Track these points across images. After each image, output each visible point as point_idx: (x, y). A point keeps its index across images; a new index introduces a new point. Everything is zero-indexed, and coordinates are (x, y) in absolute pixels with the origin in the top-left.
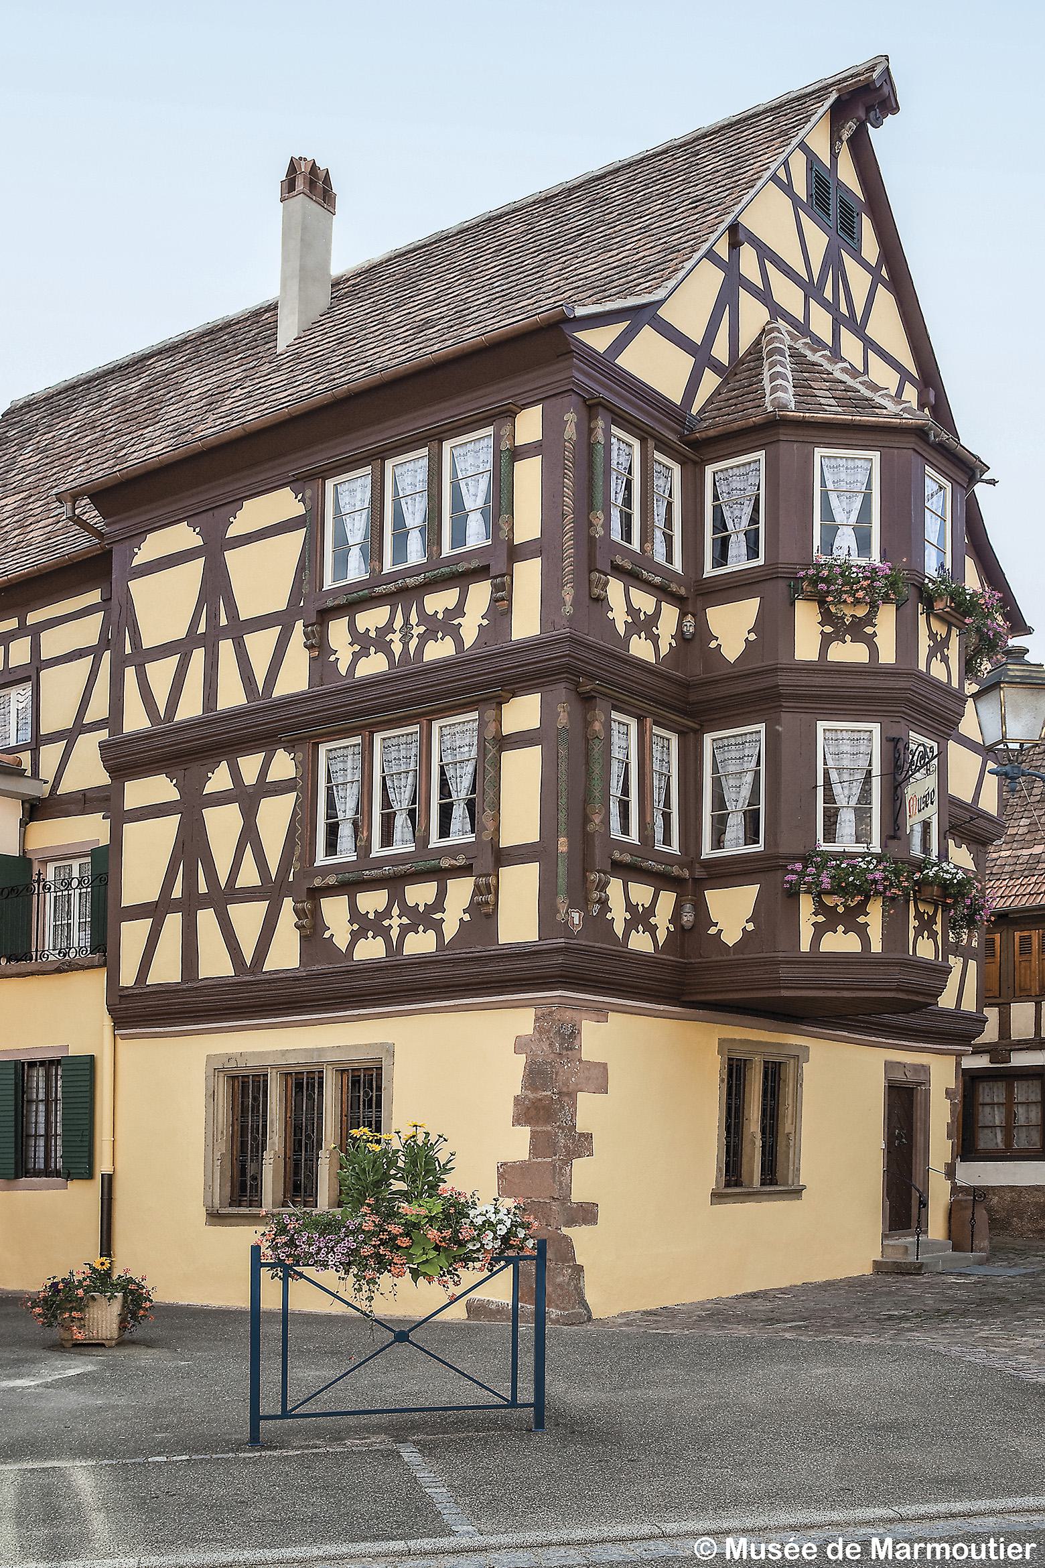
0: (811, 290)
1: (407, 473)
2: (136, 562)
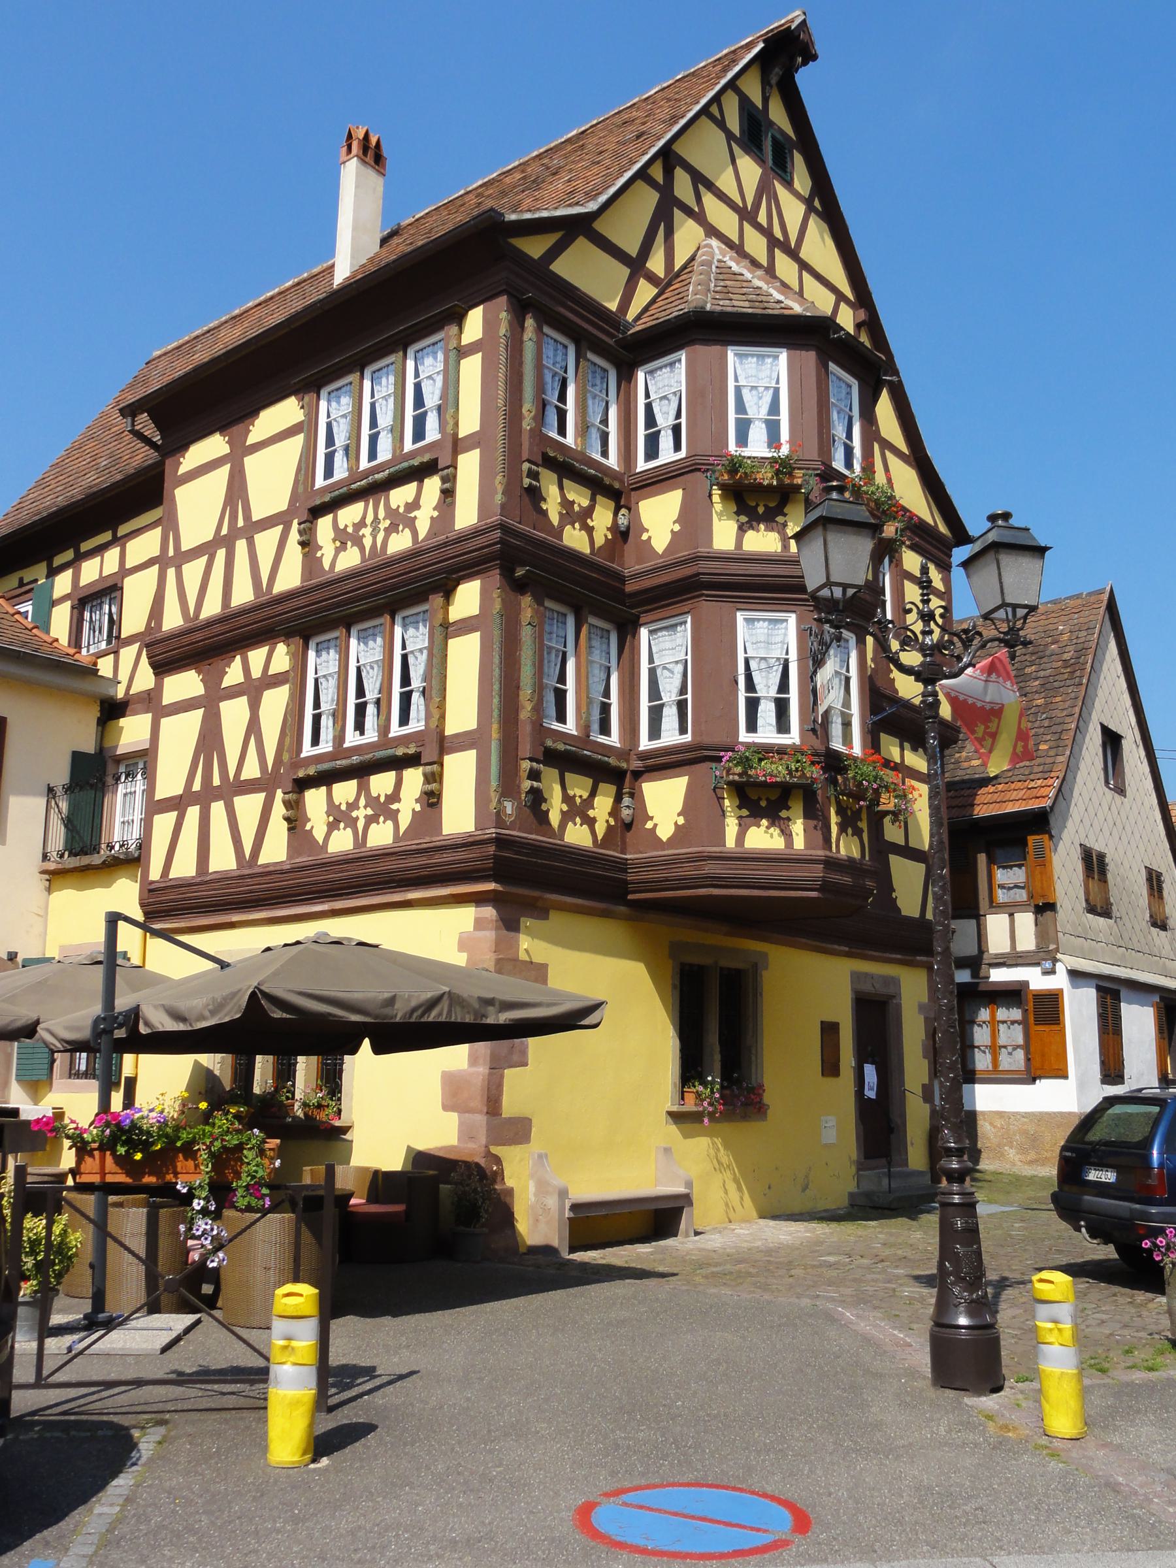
0: (747, 215)
2: (182, 470)
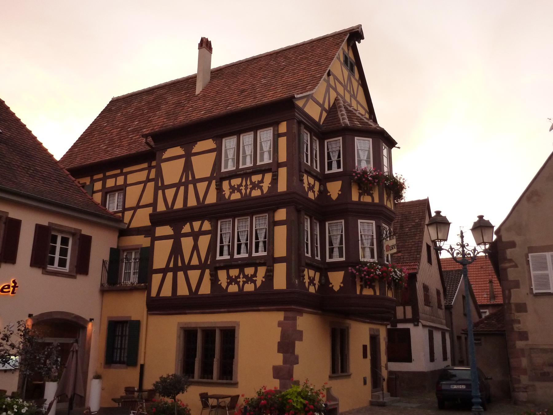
0: (345, 87)
1: (247, 139)
2: (164, 157)
